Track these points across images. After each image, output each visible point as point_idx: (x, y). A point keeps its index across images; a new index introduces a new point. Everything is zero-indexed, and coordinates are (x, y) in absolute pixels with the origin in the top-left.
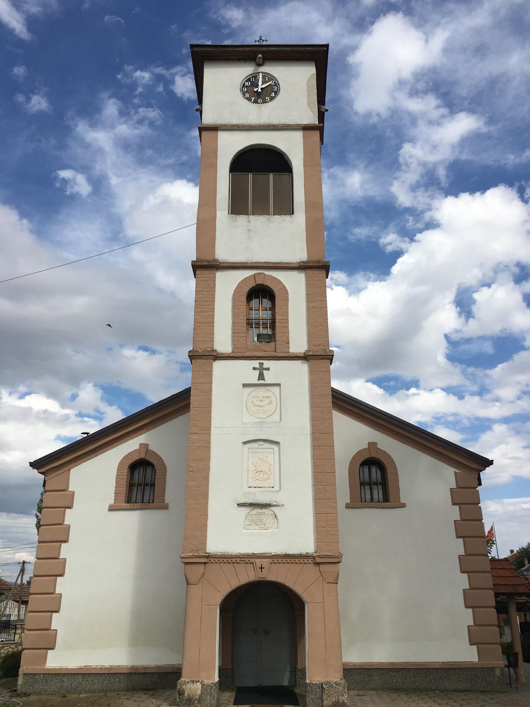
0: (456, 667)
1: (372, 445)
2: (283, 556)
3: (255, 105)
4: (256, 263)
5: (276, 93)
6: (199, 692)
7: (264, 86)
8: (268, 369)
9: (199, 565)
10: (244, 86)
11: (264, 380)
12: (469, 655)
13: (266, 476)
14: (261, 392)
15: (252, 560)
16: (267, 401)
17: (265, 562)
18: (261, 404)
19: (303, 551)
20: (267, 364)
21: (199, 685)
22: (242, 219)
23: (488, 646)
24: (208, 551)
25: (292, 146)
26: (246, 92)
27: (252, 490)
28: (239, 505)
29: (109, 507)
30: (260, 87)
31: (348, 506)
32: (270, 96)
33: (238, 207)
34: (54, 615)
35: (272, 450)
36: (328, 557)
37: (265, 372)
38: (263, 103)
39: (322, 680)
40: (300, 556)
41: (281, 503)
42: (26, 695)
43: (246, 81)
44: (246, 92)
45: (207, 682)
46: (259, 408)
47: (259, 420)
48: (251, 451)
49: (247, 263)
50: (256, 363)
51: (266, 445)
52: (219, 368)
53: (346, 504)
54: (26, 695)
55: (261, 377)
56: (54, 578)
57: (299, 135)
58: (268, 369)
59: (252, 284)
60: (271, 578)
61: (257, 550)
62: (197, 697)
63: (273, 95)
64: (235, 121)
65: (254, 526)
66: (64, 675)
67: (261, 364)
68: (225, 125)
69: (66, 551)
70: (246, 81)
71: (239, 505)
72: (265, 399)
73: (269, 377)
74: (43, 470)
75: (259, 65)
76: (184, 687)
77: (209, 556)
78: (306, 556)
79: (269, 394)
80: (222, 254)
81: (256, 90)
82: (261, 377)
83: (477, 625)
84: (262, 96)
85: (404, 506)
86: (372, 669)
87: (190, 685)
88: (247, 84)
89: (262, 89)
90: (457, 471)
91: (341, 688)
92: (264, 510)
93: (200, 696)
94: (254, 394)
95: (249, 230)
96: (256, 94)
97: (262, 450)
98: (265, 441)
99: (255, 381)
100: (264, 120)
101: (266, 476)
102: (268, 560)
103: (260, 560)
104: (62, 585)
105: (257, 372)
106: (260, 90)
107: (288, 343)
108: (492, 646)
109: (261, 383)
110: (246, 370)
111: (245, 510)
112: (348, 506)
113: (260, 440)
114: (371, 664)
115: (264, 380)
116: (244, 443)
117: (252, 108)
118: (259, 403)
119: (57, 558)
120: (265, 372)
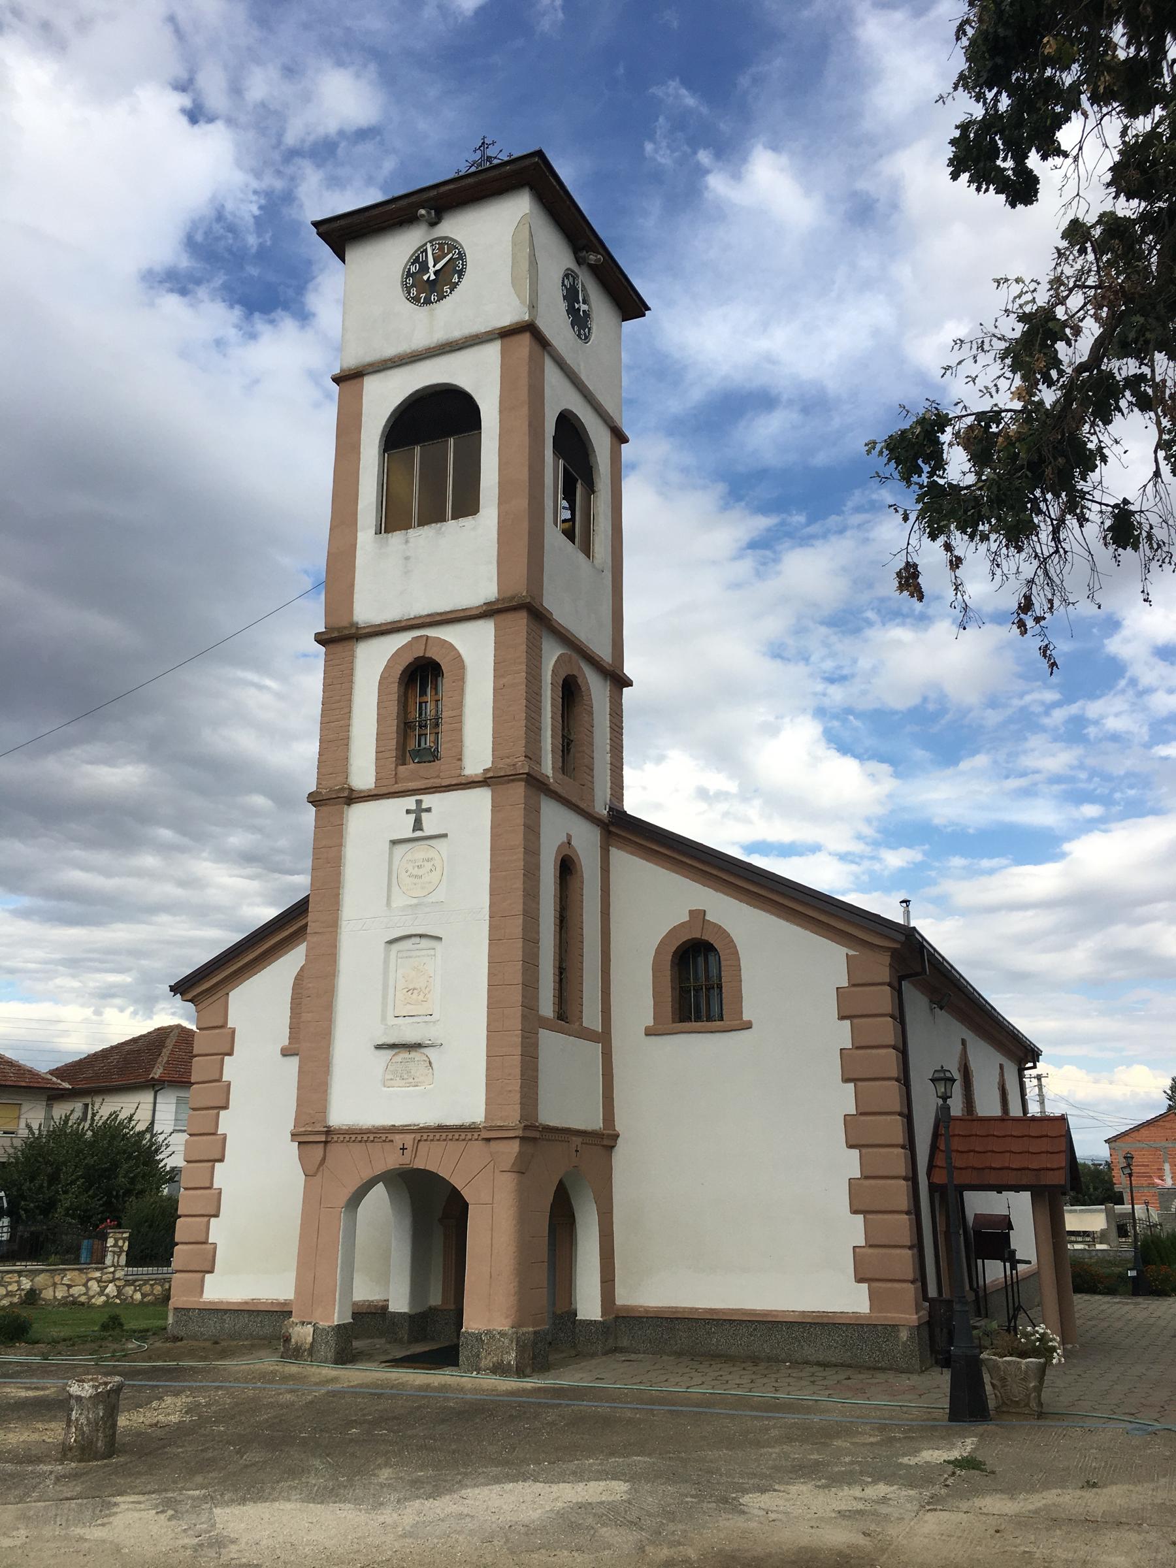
0: (825, 1321)
1: (698, 916)
2: (435, 1128)
3: (427, 308)
4: (415, 618)
5: (461, 274)
6: (310, 1339)
7: (438, 267)
8: (428, 810)
9: (315, 1146)
10: (409, 274)
11: (421, 829)
12: (855, 1301)
13: (421, 997)
14: (420, 852)
15: (390, 1137)
16: (429, 866)
17: (408, 1139)
18: (420, 872)
19: (467, 1120)
20: (428, 800)
21: (310, 1329)
22: (396, 538)
23: (889, 1285)
24: (331, 1124)
25: (480, 376)
26: (413, 286)
27: (400, 1021)
28: (379, 1047)
29: (282, 1050)
30: (432, 270)
31: (649, 1033)
32: (450, 283)
33: (393, 519)
34: (213, 1220)
35: (432, 952)
36: (501, 1128)
37: (424, 815)
38: (452, 290)
39: (483, 1328)
40: (460, 1128)
41: (439, 1042)
42: (177, 1339)
43: (413, 264)
44: (413, 286)
45: (323, 1324)
46: (416, 880)
47: (415, 901)
48: (400, 955)
49: (399, 621)
50: (410, 802)
51: (425, 943)
52: (359, 817)
53: (647, 1029)
54: (177, 1339)
55: (418, 825)
56: (210, 1164)
57: (492, 353)
58: (428, 810)
59: (408, 659)
60: (419, 1164)
61: (399, 1122)
62: (307, 1346)
63: (455, 279)
64: (390, 351)
65: (398, 1082)
66: (226, 1311)
67: (419, 802)
68: (371, 365)
69: (227, 1122)
70: (413, 264)
71: (379, 1047)
72: (425, 863)
73: (430, 825)
74: (189, 996)
75: (433, 224)
76: (291, 1330)
77: (329, 1132)
78: (471, 1128)
79: (431, 854)
80: (365, 612)
81: (425, 278)
82: (418, 825)
83: (871, 1246)
84: (438, 287)
85: (748, 1026)
86: (677, 1319)
87: (298, 1328)
88: (413, 269)
89: (436, 273)
90: (851, 953)
91: (507, 1341)
92: (413, 1054)
93: (312, 1344)
94: (409, 856)
95: (407, 558)
96: (427, 286)
97: (418, 953)
98: (421, 936)
99: (409, 834)
100: (440, 335)
101: (421, 997)
102: (413, 1136)
103: (402, 1136)
104: (222, 1176)
105: (412, 817)
106: (433, 277)
107: (460, 760)
108: (897, 1285)
109: (419, 836)
110: (392, 816)
111: (388, 1054)
112: (649, 1033)
113: (415, 935)
114: (675, 1310)
115: (421, 829)
116: (391, 942)
117: (421, 314)
118: (416, 871)
119: (214, 1134)
120: (424, 815)
